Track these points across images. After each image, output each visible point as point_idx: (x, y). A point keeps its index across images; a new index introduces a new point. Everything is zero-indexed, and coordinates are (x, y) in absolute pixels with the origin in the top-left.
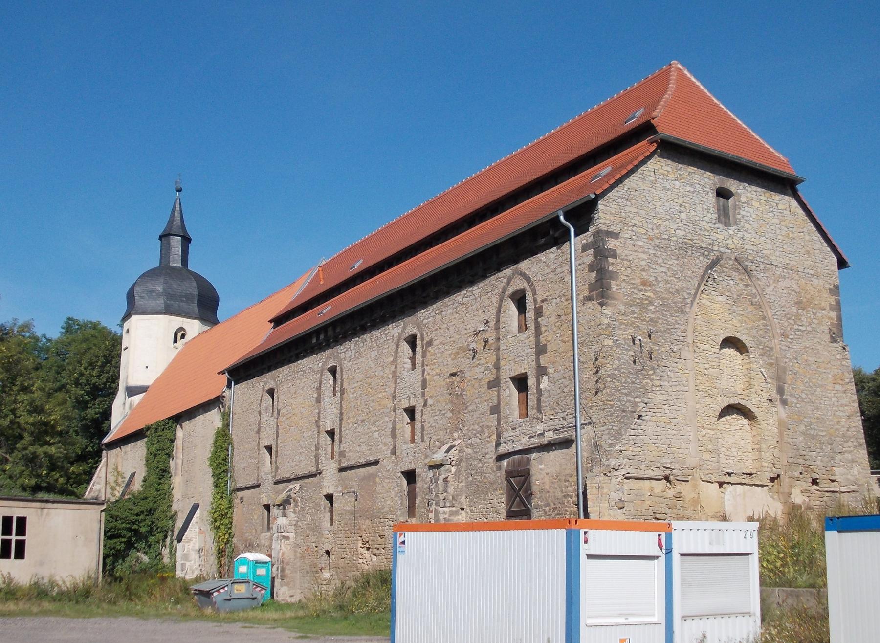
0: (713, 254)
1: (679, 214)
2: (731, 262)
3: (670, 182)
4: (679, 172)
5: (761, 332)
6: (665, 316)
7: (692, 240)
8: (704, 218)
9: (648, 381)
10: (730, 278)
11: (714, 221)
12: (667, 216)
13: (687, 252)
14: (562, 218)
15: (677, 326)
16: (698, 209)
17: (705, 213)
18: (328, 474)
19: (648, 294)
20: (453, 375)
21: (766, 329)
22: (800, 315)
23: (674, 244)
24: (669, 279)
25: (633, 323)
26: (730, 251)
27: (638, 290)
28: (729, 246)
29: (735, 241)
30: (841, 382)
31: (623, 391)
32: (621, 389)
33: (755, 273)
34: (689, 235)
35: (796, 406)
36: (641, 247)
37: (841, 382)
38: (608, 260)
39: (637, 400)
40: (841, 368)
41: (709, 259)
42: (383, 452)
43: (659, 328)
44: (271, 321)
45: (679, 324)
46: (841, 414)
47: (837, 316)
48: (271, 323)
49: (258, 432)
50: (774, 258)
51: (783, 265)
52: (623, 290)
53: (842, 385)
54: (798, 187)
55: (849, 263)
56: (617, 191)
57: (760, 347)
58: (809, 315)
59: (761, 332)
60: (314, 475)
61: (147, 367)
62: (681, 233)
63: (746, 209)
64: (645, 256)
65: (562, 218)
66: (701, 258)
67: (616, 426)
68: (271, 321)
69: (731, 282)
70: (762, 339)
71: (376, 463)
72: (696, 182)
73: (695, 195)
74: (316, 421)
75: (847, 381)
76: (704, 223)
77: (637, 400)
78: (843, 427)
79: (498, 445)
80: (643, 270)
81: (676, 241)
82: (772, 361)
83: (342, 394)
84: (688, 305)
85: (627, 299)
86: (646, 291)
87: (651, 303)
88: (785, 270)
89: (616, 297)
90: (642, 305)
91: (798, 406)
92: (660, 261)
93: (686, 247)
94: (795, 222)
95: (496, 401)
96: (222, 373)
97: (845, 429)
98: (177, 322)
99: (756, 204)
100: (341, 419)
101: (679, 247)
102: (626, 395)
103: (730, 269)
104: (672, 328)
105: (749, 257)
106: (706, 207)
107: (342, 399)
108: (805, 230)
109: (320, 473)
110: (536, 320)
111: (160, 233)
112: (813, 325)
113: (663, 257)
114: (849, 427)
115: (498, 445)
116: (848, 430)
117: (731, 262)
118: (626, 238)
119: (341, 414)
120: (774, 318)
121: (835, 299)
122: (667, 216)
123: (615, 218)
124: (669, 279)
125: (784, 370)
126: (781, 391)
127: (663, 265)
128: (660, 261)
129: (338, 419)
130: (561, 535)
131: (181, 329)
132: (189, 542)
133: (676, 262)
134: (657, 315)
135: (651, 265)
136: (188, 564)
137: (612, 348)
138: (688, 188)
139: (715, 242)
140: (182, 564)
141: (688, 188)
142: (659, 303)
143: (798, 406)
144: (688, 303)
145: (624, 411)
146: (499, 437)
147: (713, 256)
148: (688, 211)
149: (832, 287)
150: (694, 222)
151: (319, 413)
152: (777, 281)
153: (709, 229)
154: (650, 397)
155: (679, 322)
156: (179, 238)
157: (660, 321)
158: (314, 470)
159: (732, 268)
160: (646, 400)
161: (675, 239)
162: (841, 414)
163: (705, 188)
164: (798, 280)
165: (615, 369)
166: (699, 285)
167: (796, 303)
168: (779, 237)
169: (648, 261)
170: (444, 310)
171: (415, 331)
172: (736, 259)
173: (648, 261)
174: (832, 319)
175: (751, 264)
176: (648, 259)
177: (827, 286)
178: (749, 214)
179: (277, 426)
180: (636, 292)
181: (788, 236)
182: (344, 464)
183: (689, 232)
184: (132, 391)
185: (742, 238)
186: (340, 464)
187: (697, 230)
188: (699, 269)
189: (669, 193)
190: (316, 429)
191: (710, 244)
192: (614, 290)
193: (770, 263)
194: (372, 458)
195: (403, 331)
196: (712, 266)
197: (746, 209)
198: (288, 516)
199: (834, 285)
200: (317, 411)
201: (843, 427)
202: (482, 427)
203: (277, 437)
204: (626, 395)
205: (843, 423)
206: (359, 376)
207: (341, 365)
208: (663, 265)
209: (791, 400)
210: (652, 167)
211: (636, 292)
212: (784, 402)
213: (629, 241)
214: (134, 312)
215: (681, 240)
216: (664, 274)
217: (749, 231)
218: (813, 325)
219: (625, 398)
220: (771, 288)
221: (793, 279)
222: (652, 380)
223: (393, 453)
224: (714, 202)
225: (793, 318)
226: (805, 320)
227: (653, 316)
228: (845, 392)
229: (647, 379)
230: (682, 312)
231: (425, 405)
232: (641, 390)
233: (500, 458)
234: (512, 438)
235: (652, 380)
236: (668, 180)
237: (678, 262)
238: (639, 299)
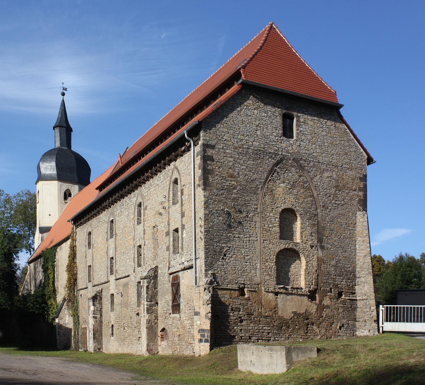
0: (278, 157)
1: (256, 131)
2: (290, 162)
3: (251, 110)
4: (257, 104)
5: (309, 205)
6: (243, 196)
7: (264, 148)
8: (273, 134)
9: (231, 234)
10: (289, 172)
11: (280, 135)
12: (247, 133)
13: (260, 156)
14: (186, 135)
15: (251, 202)
16: (269, 128)
17: (274, 130)
18: (112, 283)
19: (233, 183)
20: (154, 227)
21: (312, 203)
22: (337, 194)
23: (251, 151)
24: (247, 173)
25: (222, 200)
26: (290, 154)
27: (226, 181)
28: (290, 151)
29: (294, 148)
30: (361, 235)
31: (215, 240)
32: (213, 239)
33: (307, 168)
34: (262, 145)
35: (330, 250)
36: (229, 153)
37: (361, 235)
38: (207, 163)
39: (223, 245)
40: (362, 227)
41: (275, 160)
42: (131, 272)
43: (239, 203)
44: (97, 189)
45: (252, 201)
46: (361, 255)
47: (363, 194)
48: (97, 190)
49: (86, 257)
50: (321, 158)
51: (327, 163)
52: (216, 181)
53: (362, 237)
54: (341, 110)
55: (374, 160)
56: (215, 118)
57: (308, 214)
58: (343, 194)
59: (309, 205)
60: (107, 282)
61: (50, 215)
62: (256, 144)
63: (303, 126)
64: (232, 159)
65: (186, 135)
66: (270, 159)
67: (210, 260)
68: (97, 189)
69: (290, 174)
70: (309, 209)
71: (128, 276)
72: (269, 110)
73: (267, 118)
74: (107, 252)
75: (365, 235)
76: (273, 137)
77: (223, 245)
78: (361, 262)
79: (169, 268)
80: (230, 168)
81: (253, 149)
82: (316, 223)
83: (116, 236)
84: (259, 189)
85: (219, 186)
86: (231, 181)
87: (234, 188)
88: (328, 166)
89: (212, 185)
90: (230, 190)
91: (332, 249)
92: (242, 162)
93: (260, 152)
94: (338, 134)
95: (168, 244)
96: (69, 221)
97: (362, 264)
98: (66, 186)
99: (311, 123)
100: (116, 251)
101: (255, 153)
102: (216, 242)
103: (290, 166)
104: (248, 203)
105: (303, 158)
106: (275, 126)
107: (116, 239)
108: (345, 139)
109: (109, 282)
110: (181, 197)
111: (53, 125)
112: (346, 201)
113: (244, 159)
114: (364, 262)
115: (169, 268)
116: (363, 264)
117: (290, 162)
118: (219, 148)
119: (116, 248)
120: (318, 197)
121: (363, 184)
122: (247, 133)
123: (213, 136)
124: (247, 173)
125: (324, 228)
126: (320, 240)
127: (244, 164)
128: (242, 162)
129: (115, 251)
130: (384, 330)
131: (68, 190)
132: (61, 319)
133: (252, 162)
134: (239, 195)
135: (236, 165)
136: (61, 331)
137: (208, 215)
138: (263, 114)
139: (280, 149)
140: (58, 331)
141: (263, 114)
142: (240, 188)
143: (332, 249)
144: (259, 188)
145: (215, 251)
146: (169, 264)
147: (278, 158)
148: (262, 129)
149: (361, 176)
150: (265, 137)
151: (107, 247)
152: (322, 173)
153: (276, 140)
154: (231, 243)
155: (253, 199)
156: (65, 129)
157: (240, 199)
158: (107, 280)
159: (291, 165)
160: (229, 245)
161: (252, 148)
162: (361, 255)
163: (274, 114)
164: (338, 172)
165: (210, 228)
166: (267, 177)
167: (335, 187)
168: (326, 144)
169: (234, 162)
170: (151, 188)
171: (141, 200)
172: (294, 159)
173: (234, 162)
174: (361, 197)
175: (304, 162)
176: (234, 161)
177: (358, 175)
178: (304, 130)
179: (93, 254)
180: (225, 181)
181: (332, 143)
182: (117, 277)
183: (262, 143)
184: (43, 230)
185: (299, 145)
186: (116, 277)
187: (268, 141)
188: (268, 166)
189: (250, 118)
190: (107, 257)
191: (276, 150)
192: (210, 180)
193: (317, 161)
194: (127, 274)
195: (137, 200)
196: (276, 165)
197: (303, 126)
198: (96, 305)
199: (363, 174)
200: (107, 246)
201: (361, 262)
202: (164, 258)
203: (93, 260)
204: (216, 242)
205: (361, 260)
206: (122, 226)
207: (115, 219)
208: (244, 164)
209: (326, 245)
210: (239, 101)
211: (225, 181)
212: (322, 248)
213: (221, 150)
214: (40, 179)
215: (256, 148)
216: (244, 170)
217: (304, 141)
218: (346, 201)
219: (216, 244)
220: (318, 177)
221: (333, 171)
222: (233, 234)
223: (134, 272)
224: (281, 122)
225: (332, 196)
226: (341, 197)
227: (235, 196)
228: (363, 241)
229: (231, 233)
230: (255, 193)
231: (145, 245)
232: (227, 240)
233: (170, 274)
234: (174, 265)
235: (233, 234)
236: (249, 110)
237: (254, 163)
238: (227, 186)
